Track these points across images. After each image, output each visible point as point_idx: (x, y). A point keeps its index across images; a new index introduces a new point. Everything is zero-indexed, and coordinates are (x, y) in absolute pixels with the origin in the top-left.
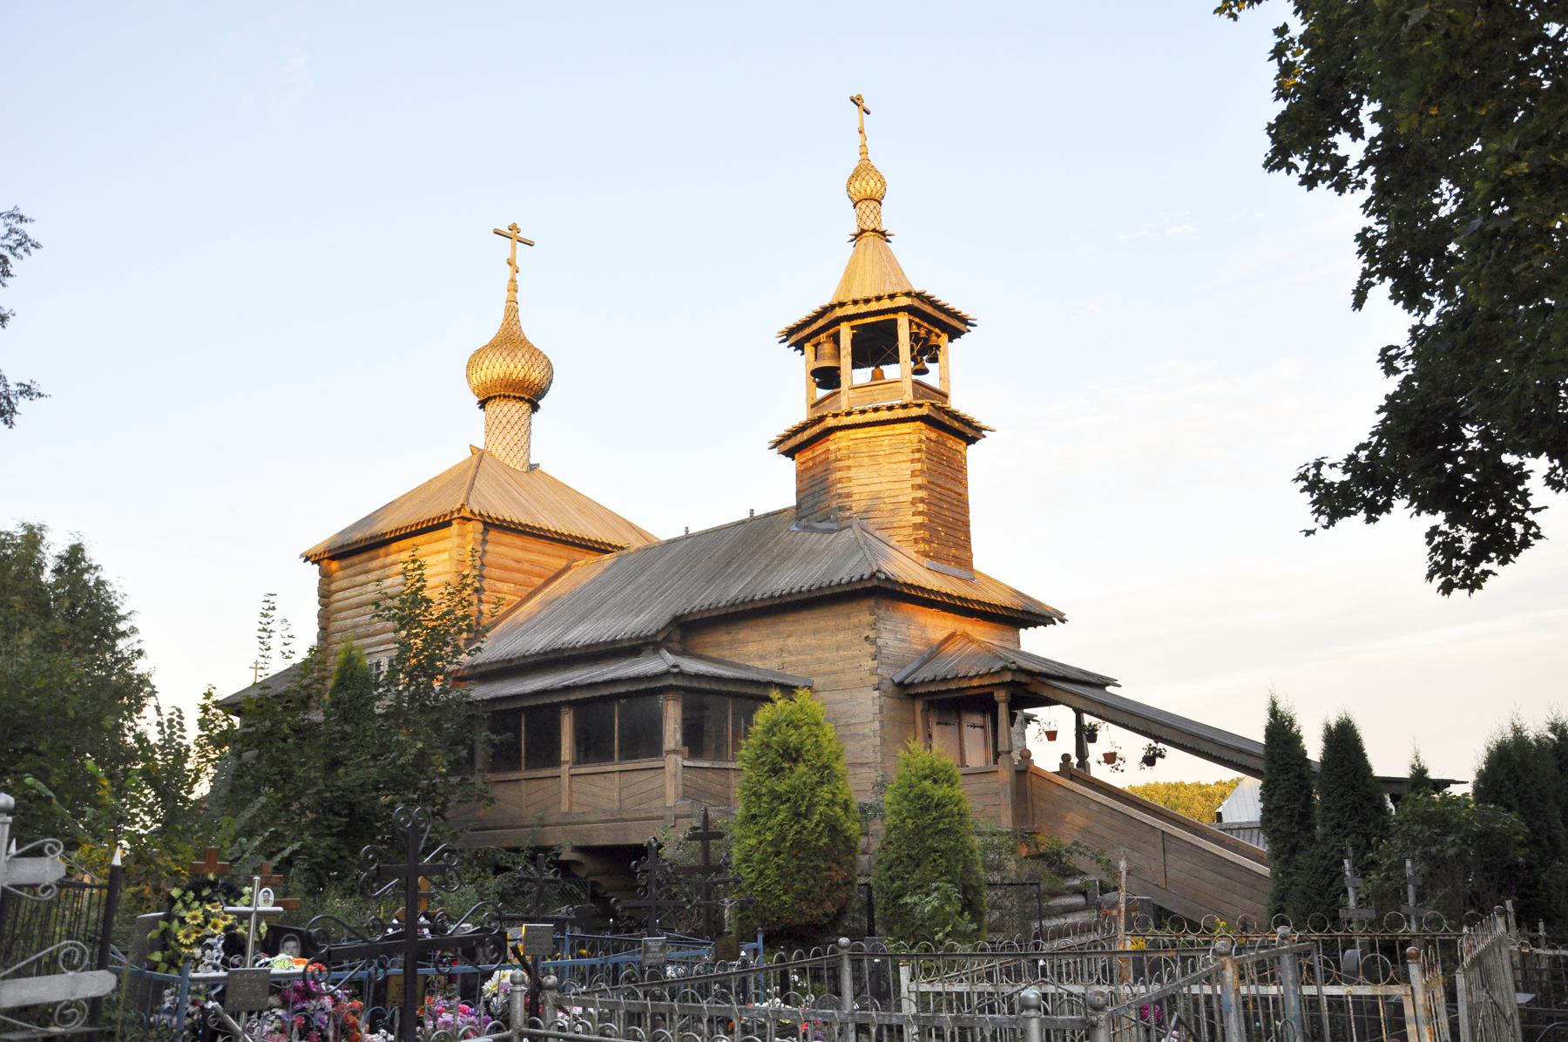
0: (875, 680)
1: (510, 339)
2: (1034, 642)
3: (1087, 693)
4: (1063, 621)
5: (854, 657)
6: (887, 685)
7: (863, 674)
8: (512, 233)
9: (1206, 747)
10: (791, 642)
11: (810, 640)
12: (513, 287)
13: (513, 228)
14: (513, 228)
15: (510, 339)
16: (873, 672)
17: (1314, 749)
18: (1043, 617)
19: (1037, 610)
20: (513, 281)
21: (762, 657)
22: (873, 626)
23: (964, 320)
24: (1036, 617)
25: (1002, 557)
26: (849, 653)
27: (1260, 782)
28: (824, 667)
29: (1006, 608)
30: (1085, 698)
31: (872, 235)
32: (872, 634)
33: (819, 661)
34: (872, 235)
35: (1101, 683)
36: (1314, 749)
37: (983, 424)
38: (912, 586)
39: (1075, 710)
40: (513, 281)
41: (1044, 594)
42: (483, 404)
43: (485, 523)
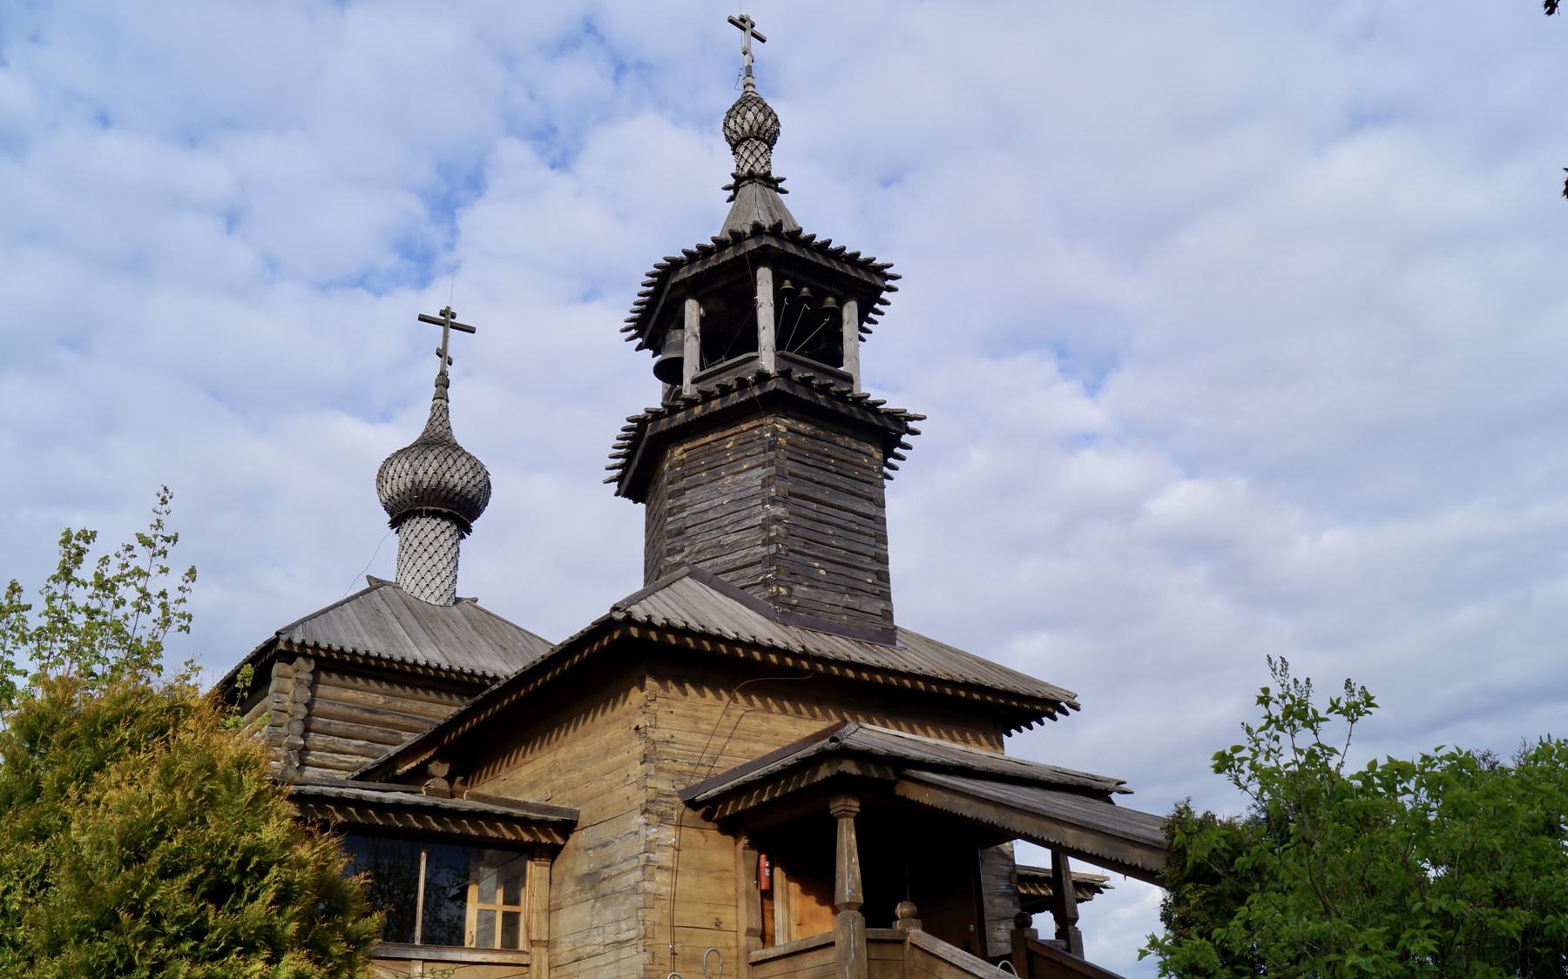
0: (641, 798)
1: (437, 440)
2: (1026, 747)
4: (1076, 707)
5: (622, 765)
6: (677, 809)
7: (629, 790)
8: (446, 320)
11: (579, 747)
12: (443, 382)
15: (437, 440)
17: (1057, 714)
20: (443, 374)
21: (533, 786)
23: (879, 271)
24: (1028, 707)
28: (593, 788)
30: (998, 804)
31: (755, 180)
32: (641, 721)
33: (588, 780)
34: (755, 180)
35: (1095, 791)
36: (1057, 714)
37: (892, 404)
40: (443, 374)
41: (1027, 658)
42: (396, 523)
43: (317, 658)
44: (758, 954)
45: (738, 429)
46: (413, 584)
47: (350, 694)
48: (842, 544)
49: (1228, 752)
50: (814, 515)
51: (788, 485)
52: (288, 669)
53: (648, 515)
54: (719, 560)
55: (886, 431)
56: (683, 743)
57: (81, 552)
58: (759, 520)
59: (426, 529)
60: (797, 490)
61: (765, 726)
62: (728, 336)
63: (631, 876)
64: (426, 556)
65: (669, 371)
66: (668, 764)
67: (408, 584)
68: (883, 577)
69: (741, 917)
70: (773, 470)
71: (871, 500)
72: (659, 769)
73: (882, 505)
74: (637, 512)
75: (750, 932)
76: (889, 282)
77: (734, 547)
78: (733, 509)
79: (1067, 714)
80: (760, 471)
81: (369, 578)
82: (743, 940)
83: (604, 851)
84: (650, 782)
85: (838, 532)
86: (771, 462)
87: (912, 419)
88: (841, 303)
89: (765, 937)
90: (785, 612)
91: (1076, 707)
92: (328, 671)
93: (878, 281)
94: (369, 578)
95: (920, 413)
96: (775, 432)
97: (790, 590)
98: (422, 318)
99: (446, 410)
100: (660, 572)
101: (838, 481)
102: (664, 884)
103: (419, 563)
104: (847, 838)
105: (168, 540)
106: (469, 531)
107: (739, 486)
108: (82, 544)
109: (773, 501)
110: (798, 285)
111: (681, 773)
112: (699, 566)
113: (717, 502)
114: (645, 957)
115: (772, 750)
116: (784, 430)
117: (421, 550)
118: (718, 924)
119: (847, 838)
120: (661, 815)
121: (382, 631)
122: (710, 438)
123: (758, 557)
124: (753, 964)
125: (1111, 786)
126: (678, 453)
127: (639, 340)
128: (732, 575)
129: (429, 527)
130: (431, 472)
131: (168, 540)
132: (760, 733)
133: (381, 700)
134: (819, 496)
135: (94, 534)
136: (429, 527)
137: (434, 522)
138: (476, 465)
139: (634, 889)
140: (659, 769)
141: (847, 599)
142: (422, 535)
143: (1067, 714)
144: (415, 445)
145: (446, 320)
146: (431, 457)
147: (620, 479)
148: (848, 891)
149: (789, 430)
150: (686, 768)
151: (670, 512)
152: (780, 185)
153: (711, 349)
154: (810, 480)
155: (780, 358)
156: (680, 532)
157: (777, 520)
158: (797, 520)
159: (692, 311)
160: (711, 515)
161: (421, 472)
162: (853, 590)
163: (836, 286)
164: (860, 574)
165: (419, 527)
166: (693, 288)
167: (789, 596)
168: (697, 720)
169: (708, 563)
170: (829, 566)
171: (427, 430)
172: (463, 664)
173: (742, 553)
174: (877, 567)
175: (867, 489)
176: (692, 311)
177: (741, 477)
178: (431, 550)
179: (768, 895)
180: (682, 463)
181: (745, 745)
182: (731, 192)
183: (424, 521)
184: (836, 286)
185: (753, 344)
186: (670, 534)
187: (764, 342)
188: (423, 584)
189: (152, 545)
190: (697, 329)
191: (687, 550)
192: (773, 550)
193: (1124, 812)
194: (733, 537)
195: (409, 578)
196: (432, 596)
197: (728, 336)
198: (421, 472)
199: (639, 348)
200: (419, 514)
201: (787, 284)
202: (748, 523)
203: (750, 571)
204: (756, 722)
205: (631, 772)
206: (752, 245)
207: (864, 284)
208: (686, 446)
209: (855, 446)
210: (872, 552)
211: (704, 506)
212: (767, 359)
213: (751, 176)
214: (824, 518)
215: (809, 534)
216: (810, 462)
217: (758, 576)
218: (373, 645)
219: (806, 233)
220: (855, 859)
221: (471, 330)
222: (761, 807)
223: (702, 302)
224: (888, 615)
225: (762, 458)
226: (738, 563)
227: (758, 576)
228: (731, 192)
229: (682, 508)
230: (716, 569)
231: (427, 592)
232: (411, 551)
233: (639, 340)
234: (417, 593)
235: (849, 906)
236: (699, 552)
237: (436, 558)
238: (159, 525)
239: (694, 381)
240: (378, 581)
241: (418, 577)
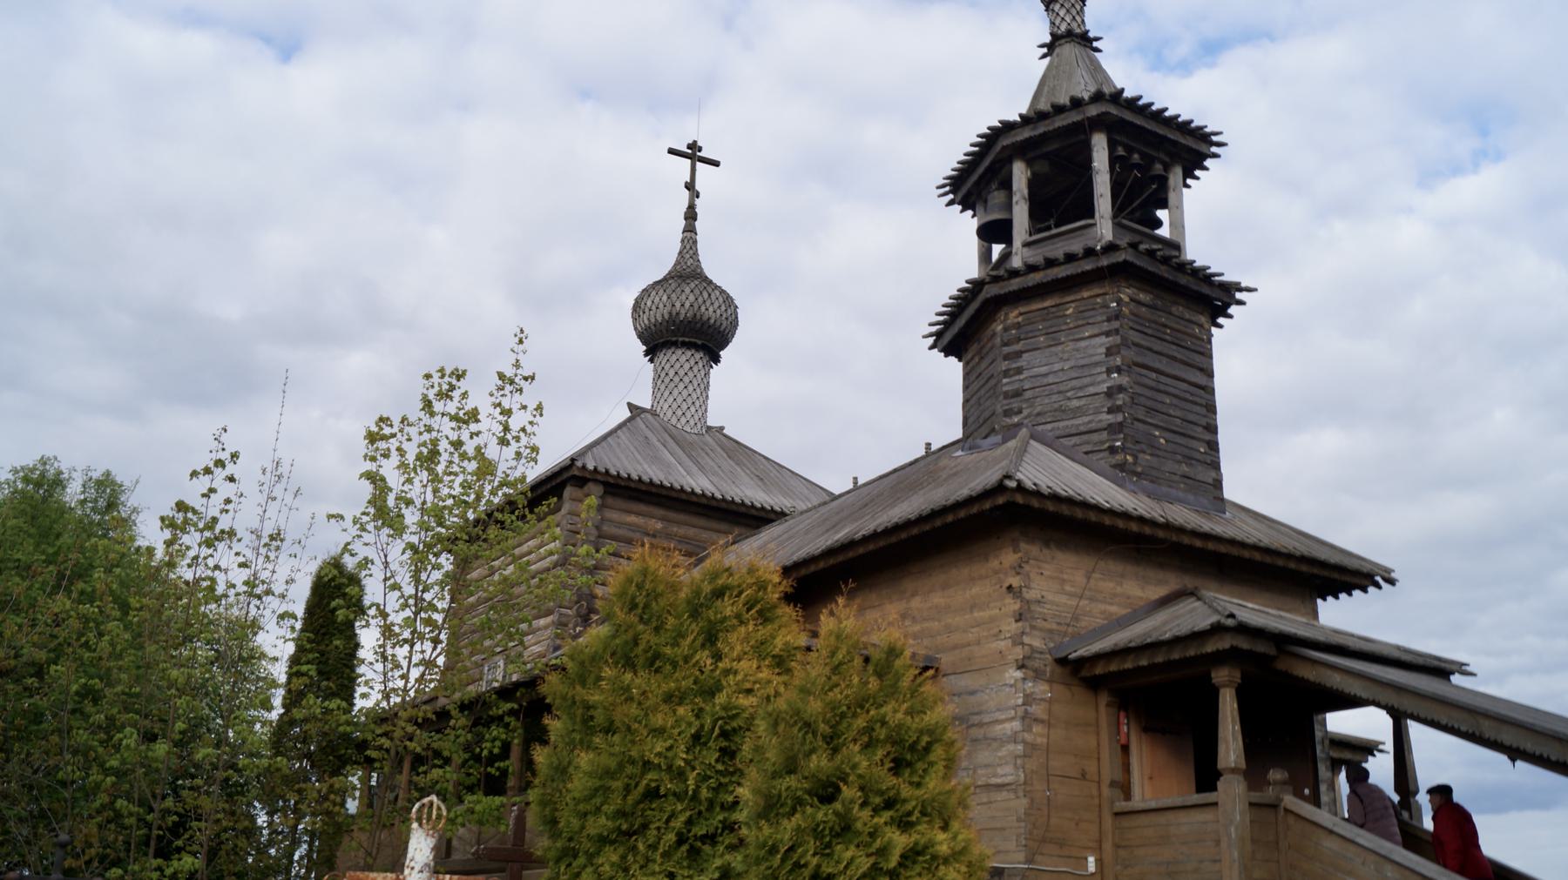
0: (1019, 652)
1: (687, 272)
2: (1339, 615)
3: (1421, 688)
4: (1392, 582)
5: (992, 620)
6: (1045, 663)
7: (1002, 645)
8: (693, 153)
9: (1488, 729)
10: (916, 603)
11: (937, 599)
12: (691, 215)
13: (694, 146)
14: (694, 146)
15: (687, 272)
16: (1017, 640)
18: (1357, 573)
19: (1354, 564)
22: (1018, 569)
24: (1350, 576)
25: (1273, 472)
26: (985, 614)
27: (1371, 780)
28: (956, 638)
29: (1267, 551)
32: (1015, 581)
33: (949, 630)
35: (1440, 670)
37: (1228, 277)
38: (1069, 501)
39: (1391, 711)
43: (605, 484)
44: (1122, 805)
45: (1078, 296)
46: (670, 413)
47: (632, 519)
48: (1178, 413)
49: (374, 429)
50: (1153, 384)
51: (1131, 354)
52: (578, 493)
53: (966, 376)
54: (1061, 424)
55: (1213, 297)
56: (1052, 603)
57: (452, 388)
58: (1104, 388)
59: (680, 359)
60: (1139, 360)
61: (1119, 590)
62: (1061, 201)
63: (1007, 726)
64: (681, 386)
65: (992, 232)
66: (1040, 623)
67: (665, 410)
68: (1213, 446)
69: (1109, 769)
70: (1118, 339)
71: (1201, 370)
72: (1033, 627)
73: (1210, 375)
74: (952, 370)
75: (1113, 784)
76: (1214, 149)
77: (1077, 413)
78: (1074, 375)
79: (1379, 587)
80: (1103, 339)
81: (629, 405)
82: (1106, 791)
83: (972, 699)
84: (1026, 640)
85: (1175, 401)
86: (1117, 331)
87: (1241, 290)
88: (1167, 168)
89: (1126, 790)
90: (1122, 472)
91: (1392, 582)
92: (614, 495)
93: (1203, 148)
94: (629, 405)
95: (1251, 285)
96: (1119, 301)
97: (1135, 457)
98: (672, 151)
99: (695, 242)
100: (993, 430)
101: (1173, 351)
102: (1041, 735)
103: (676, 392)
104: (1228, 706)
105: (526, 379)
106: (716, 359)
107: (1076, 356)
108: (454, 382)
109: (1119, 370)
110: (1130, 150)
111: (1051, 631)
112: (1040, 428)
113: (1057, 367)
114: (1025, 801)
115: (1124, 612)
116: (1127, 299)
117: (677, 379)
118: (1084, 775)
119: (1228, 706)
120: (1036, 671)
121: (656, 459)
122: (1047, 303)
123: (1104, 425)
124: (1117, 814)
125: (1454, 667)
126: (1014, 315)
127: (951, 196)
128: (1075, 440)
129: (683, 359)
130: (687, 305)
131: (526, 379)
132: (1115, 595)
133: (659, 525)
134: (1157, 365)
135: (464, 372)
136: (683, 359)
137: (689, 353)
138: (728, 301)
139: (1014, 738)
140: (1033, 627)
141: (1184, 468)
142: (678, 365)
143: (1379, 587)
144: (665, 279)
145: (693, 153)
146: (687, 290)
147: (939, 335)
148: (1232, 757)
149: (1132, 300)
150: (1054, 626)
151: (1006, 373)
152: (1095, 44)
153: (1040, 215)
154: (1150, 350)
155: (1117, 225)
156: (1018, 394)
157: (1121, 389)
158: (1139, 390)
159: (1020, 174)
160: (1051, 379)
161: (678, 305)
162: (1189, 459)
163: (1166, 150)
164: (1194, 444)
165: (674, 357)
166: (1023, 150)
167: (1135, 463)
168: (1063, 581)
169: (1049, 427)
170: (1167, 435)
171: (677, 263)
172: (694, 485)
173: (1086, 419)
174: (1207, 437)
175: (1198, 359)
176: (1020, 174)
177: (1083, 344)
178: (686, 380)
179: (1125, 749)
180: (1018, 326)
181: (1102, 607)
182: (1045, 50)
183: (679, 352)
184: (1166, 150)
185: (1089, 211)
186: (1007, 395)
187: (1083, 208)
188: (679, 413)
189: (512, 382)
190: (1026, 192)
191: (1025, 412)
192: (1120, 418)
193: (1457, 687)
194: (1075, 403)
195: (666, 406)
196: (687, 425)
197: (1061, 201)
198: (678, 305)
199: (950, 203)
200: (675, 344)
201: (1121, 151)
202: (1092, 390)
203: (1095, 437)
204: (1111, 585)
205: (1004, 628)
206: (1093, 111)
207: (1189, 147)
208: (1022, 309)
209: (1187, 316)
210: (1203, 422)
211: (1044, 370)
212: (1104, 228)
213: (1070, 34)
214: (1162, 387)
215: (1149, 403)
216: (1150, 331)
217: (1102, 443)
218: (654, 473)
219: (1127, 94)
220: (1238, 727)
221: (716, 164)
222: (1139, 669)
223: (1029, 163)
224: (1218, 484)
225: (1106, 327)
226: (1082, 429)
227: (1102, 443)
228: (1045, 50)
229: (1019, 371)
230: (1058, 433)
231: (683, 420)
232: (667, 380)
233: (951, 196)
234: (674, 421)
235: (1233, 771)
236: (1039, 414)
237: (691, 388)
238: (517, 365)
239: (1026, 245)
240: (637, 408)
241: (675, 406)
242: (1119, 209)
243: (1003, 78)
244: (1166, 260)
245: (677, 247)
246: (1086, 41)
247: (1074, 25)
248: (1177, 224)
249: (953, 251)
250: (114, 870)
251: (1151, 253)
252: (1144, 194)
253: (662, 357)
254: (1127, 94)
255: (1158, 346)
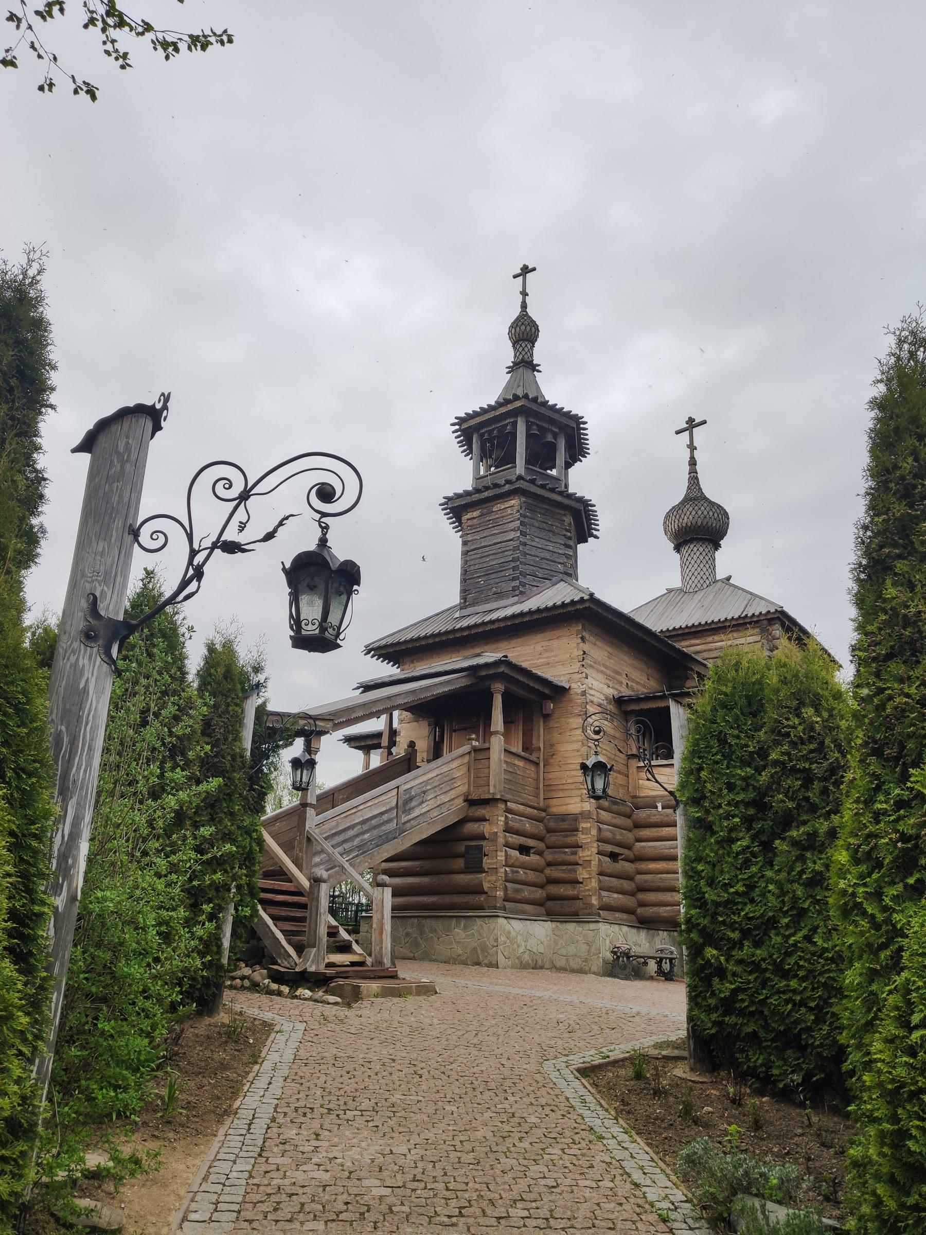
1: (695, 495)
12: (693, 462)
15: (695, 495)
59: (696, 550)
99: (697, 478)
136: (695, 549)
185: (513, 461)
242: (528, 462)
243: (486, 390)
244: (561, 493)
245: (686, 484)
246: (533, 367)
247: (526, 357)
248: (476, 469)
249: (461, 473)
250: (913, 1149)
251: (543, 487)
252: (542, 456)
253: (684, 550)
254: (550, 403)
255: (486, 533)
